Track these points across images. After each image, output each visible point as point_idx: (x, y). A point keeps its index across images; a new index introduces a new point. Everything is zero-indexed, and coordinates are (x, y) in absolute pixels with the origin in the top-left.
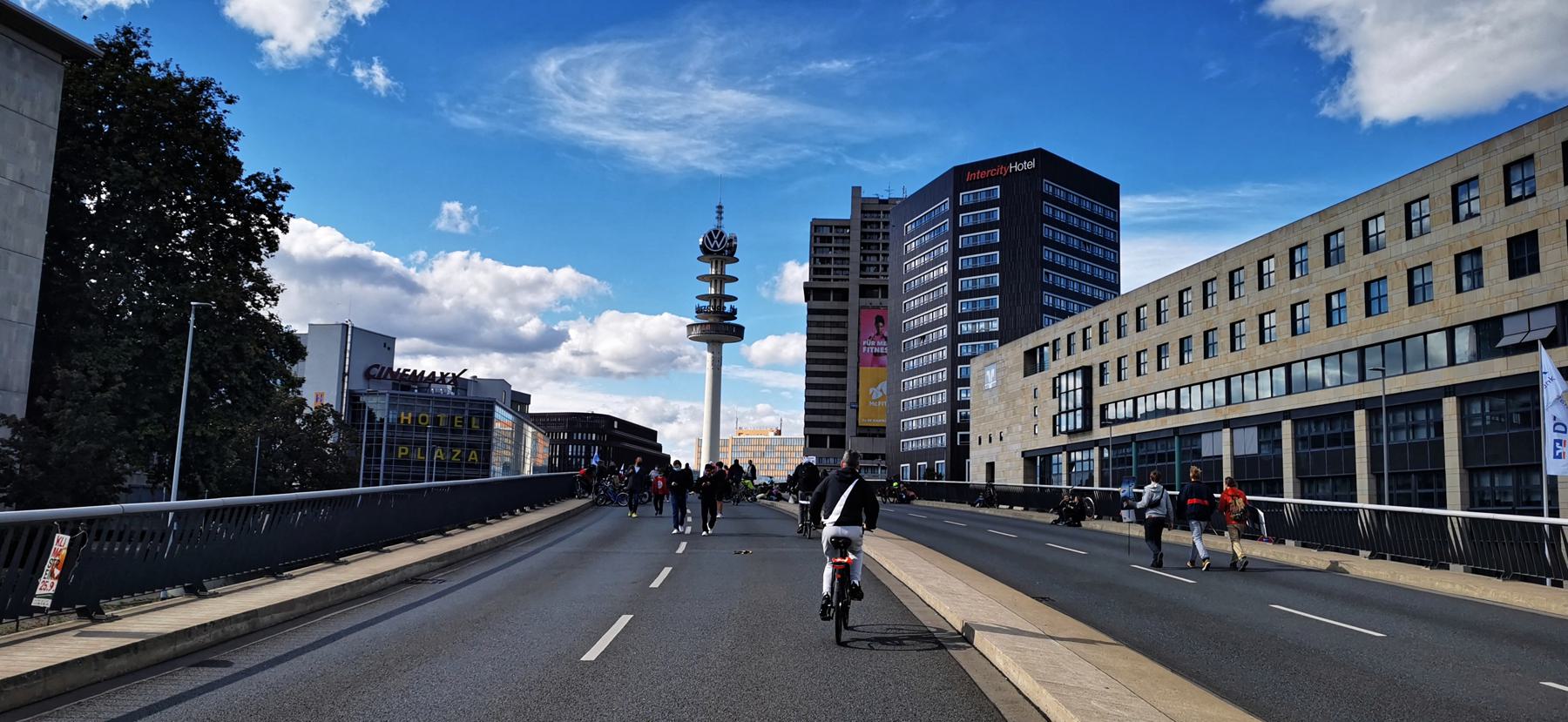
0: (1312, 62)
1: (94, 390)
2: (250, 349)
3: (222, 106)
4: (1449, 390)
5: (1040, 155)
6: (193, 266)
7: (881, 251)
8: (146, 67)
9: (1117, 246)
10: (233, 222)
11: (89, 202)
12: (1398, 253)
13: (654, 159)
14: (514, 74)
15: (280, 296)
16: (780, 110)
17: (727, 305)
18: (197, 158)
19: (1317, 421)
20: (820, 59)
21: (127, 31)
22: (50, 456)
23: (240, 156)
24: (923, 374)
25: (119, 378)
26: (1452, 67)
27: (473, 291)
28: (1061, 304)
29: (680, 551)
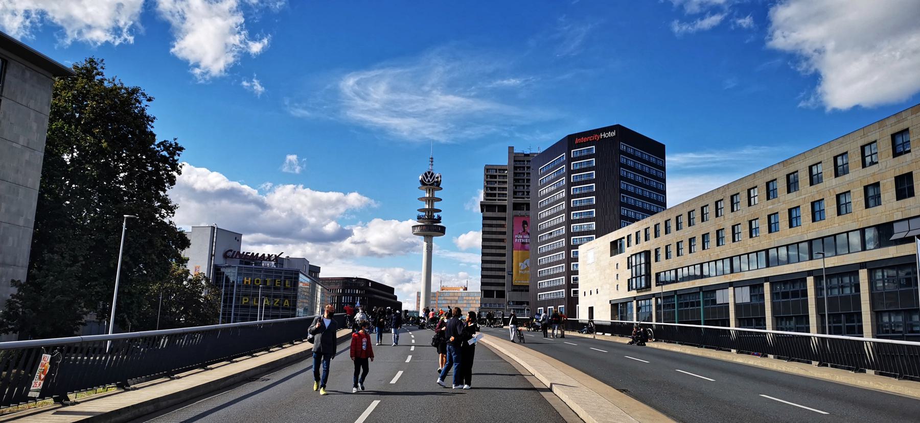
0: (799, 76)
1: (67, 265)
2: (158, 242)
3: (144, 102)
4: (863, 265)
5: (618, 128)
6: (126, 193)
7: (526, 183)
8: (101, 81)
9: (664, 181)
10: (150, 168)
11: (66, 158)
12: (831, 185)
13: (405, 134)
14: (329, 86)
15: (176, 211)
16: (479, 106)
17: (436, 215)
18: (130, 132)
19: (785, 283)
20: (503, 78)
21: (92, 61)
22: (42, 307)
23: (154, 131)
24: (549, 252)
25: (81, 259)
26: (876, 78)
27: (299, 206)
28: (632, 214)
29: (408, 361)
